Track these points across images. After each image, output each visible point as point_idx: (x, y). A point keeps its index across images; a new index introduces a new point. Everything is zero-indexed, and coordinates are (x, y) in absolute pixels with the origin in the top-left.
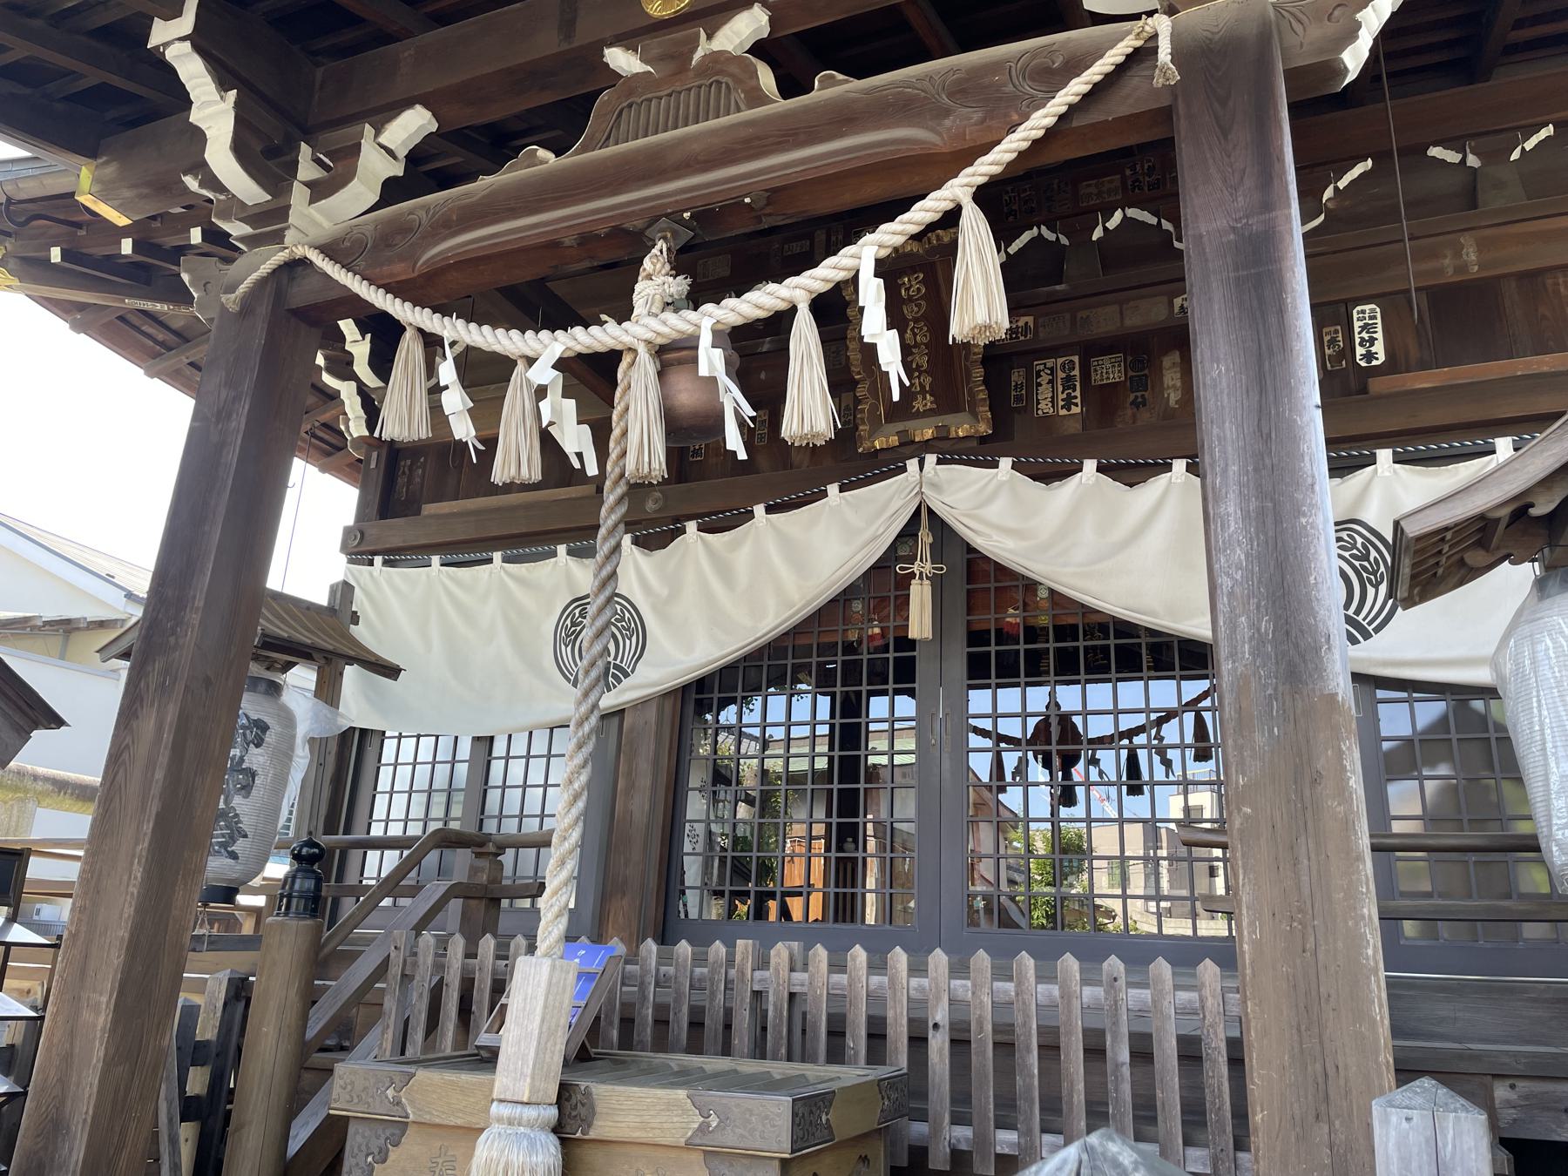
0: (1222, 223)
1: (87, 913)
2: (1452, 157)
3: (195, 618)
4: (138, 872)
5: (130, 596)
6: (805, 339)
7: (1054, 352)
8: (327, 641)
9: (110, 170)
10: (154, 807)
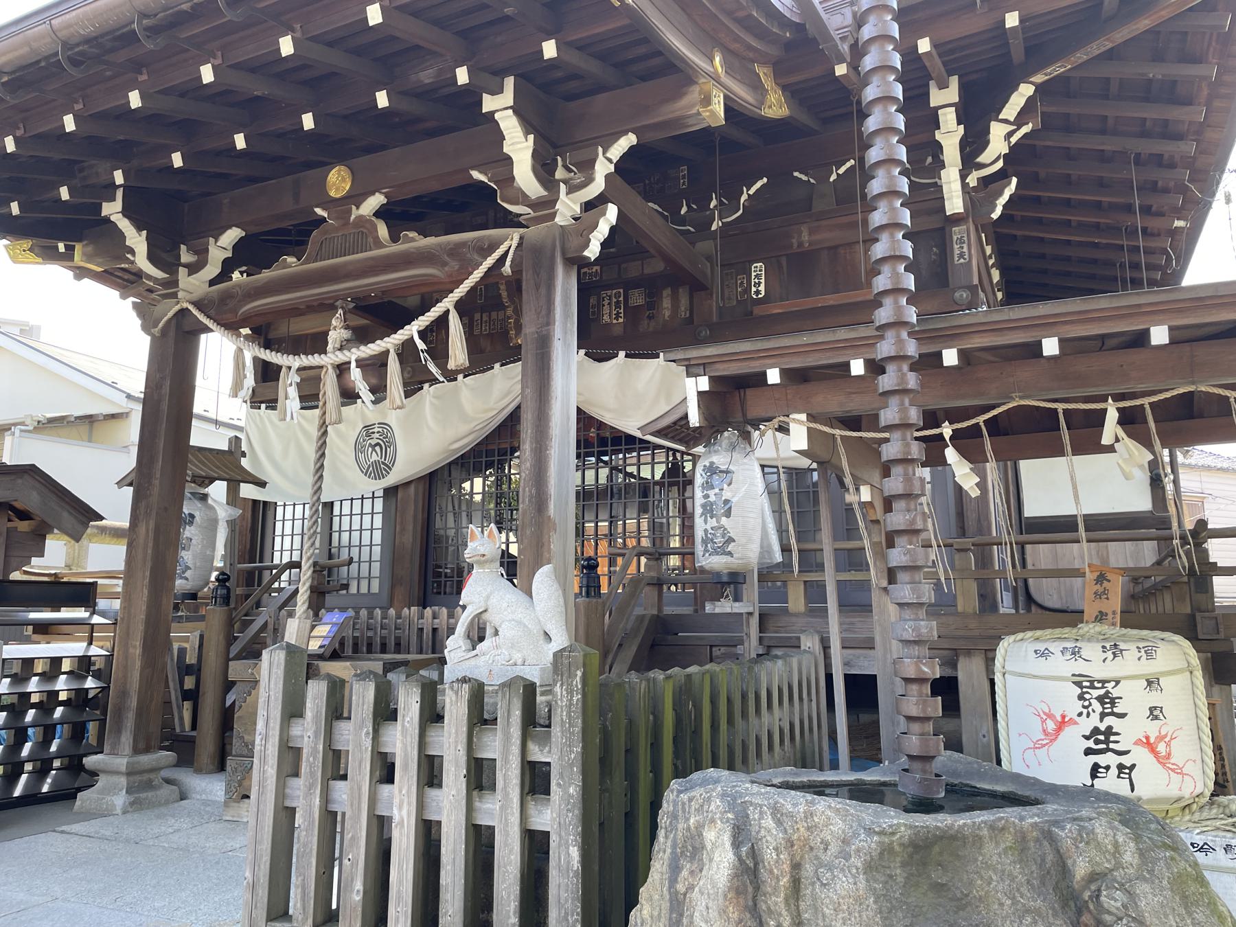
0: (533, 329)
1: (127, 606)
2: (804, 178)
3: (157, 482)
4: (146, 592)
5: (129, 396)
6: (393, 365)
7: (611, 287)
8: (228, 464)
9: (90, 249)
10: (149, 564)
